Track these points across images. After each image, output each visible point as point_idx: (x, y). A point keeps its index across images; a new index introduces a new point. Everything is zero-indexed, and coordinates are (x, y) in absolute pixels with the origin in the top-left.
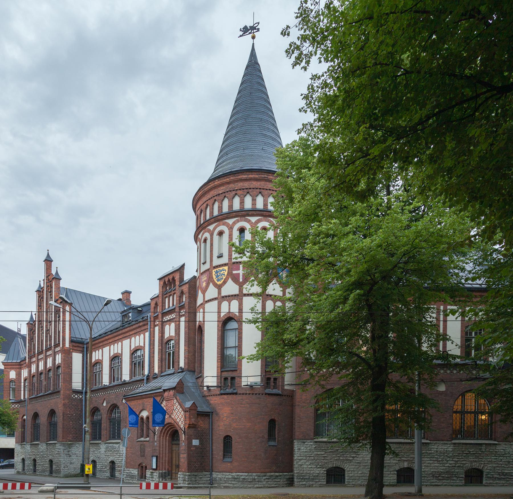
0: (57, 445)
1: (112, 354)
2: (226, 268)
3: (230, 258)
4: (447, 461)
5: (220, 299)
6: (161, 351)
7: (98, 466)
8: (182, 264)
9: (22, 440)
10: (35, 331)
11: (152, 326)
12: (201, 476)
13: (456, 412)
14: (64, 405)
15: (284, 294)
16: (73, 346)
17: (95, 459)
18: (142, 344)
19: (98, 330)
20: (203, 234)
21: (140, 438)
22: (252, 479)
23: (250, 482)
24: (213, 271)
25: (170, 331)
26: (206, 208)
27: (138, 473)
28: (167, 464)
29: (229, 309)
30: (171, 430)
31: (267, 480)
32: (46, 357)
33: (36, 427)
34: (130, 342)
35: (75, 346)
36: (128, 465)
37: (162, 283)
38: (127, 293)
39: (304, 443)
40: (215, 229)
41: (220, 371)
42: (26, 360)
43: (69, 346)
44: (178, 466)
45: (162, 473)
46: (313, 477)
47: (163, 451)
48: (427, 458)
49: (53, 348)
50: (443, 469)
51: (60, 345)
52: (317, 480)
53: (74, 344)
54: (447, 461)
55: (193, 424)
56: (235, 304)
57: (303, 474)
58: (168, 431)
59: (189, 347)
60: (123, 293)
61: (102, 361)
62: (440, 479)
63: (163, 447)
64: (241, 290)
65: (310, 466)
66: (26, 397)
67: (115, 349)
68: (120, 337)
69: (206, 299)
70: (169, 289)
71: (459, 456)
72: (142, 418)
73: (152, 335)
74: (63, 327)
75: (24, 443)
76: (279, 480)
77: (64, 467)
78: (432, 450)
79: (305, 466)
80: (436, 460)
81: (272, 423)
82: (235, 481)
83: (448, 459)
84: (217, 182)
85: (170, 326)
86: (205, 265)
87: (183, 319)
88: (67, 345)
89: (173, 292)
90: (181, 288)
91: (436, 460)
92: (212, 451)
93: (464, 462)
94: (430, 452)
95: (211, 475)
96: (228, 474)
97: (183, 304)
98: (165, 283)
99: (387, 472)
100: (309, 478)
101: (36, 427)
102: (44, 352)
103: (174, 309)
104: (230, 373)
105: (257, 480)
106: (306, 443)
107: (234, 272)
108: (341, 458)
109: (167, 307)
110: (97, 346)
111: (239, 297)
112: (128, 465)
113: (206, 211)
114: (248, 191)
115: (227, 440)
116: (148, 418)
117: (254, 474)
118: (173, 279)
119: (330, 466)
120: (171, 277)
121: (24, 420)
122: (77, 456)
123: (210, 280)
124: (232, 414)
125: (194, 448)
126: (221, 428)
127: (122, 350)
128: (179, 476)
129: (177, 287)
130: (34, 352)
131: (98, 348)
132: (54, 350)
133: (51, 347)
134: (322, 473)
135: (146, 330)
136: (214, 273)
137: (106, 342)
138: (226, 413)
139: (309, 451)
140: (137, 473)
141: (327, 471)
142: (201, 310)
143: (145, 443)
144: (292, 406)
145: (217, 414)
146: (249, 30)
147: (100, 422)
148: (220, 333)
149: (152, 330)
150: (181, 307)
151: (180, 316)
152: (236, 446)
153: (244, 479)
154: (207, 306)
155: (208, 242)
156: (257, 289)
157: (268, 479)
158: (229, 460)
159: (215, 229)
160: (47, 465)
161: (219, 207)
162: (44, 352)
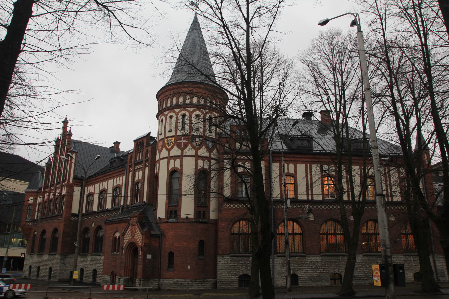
0: (56, 256)
1: (101, 189)
2: (173, 138)
3: (176, 133)
4: (318, 269)
5: (170, 158)
6: (132, 189)
7: (85, 273)
8: (149, 132)
9: (31, 251)
10: (50, 169)
11: (128, 172)
12: (152, 282)
13: (322, 234)
14: (65, 225)
15: (210, 155)
16: (75, 182)
17: (83, 267)
18: (121, 184)
19: (91, 173)
20: (161, 116)
21: (114, 252)
22: (187, 283)
23: (185, 286)
24: (166, 140)
25: (139, 176)
26: (163, 102)
27: (110, 279)
28: (130, 272)
29: (175, 165)
30: (134, 247)
31: (197, 285)
32: (56, 189)
33: (43, 241)
34: (113, 182)
35: (77, 182)
36: (104, 273)
37: (136, 144)
38: (117, 144)
39: (223, 257)
40: (168, 114)
41: (167, 206)
42: (42, 189)
43: (73, 182)
44: (136, 274)
45: (126, 279)
46: (229, 282)
47: (127, 262)
48: (305, 267)
49: (61, 183)
50: (315, 275)
51: (66, 181)
52: (232, 284)
53: (76, 180)
54: (318, 269)
55: (147, 243)
56: (178, 161)
57: (223, 280)
58: (131, 248)
59: (149, 188)
60: (114, 143)
61: (94, 193)
62: (314, 282)
63: (127, 260)
64: (182, 153)
65: (227, 274)
66: (39, 217)
67: (103, 185)
68: (107, 177)
69: (161, 157)
70: (140, 148)
71: (326, 265)
72: (116, 237)
73: (127, 178)
74: (69, 169)
75: (33, 253)
76: (206, 284)
77: (60, 273)
78: (308, 261)
79: (224, 274)
80: (311, 268)
81: (202, 243)
82: (175, 285)
83: (319, 267)
84: (170, 88)
85: (139, 172)
86: (161, 135)
87: (147, 169)
88: (71, 181)
89: (142, 150)
90: (147, 148)
91: (311, 268)
92: (161, 263)
93: (329, 269)
94: (307, 262)
95: (159, 280)
96: (170, 280)
97: (147, 158)
98: (137, 143)
99: (279, 278)
100: (227, 283)
101: (43, 241)
102: (55, 185)
103: (142, 161)
104: (174, 207)
105: (190, 285)
106: (224, 258)
107: (179, 141)
108: (248, 268)
109: (138, 160)
110: (92, 182)
111: (181, 157)
112: (104, 273)
113: (163, 103)
114: (187, 93)
115: (171, 255)
116: (119, 237)
117: (188, 280)
118: (143, 141)
119: (241, 274)
120: (141, 140)
121: (35, 235)
122: (70, 265)
123: (163, 145)
124: (175, 236)
125: (148, 261)
126: (167, 246)
127: (108, 186)
128: (136, 281)
129: (145, 147)
130: (48, 184)
131: (92, 184)
132: (62, 184)
133: (60, 182)
134: (236, 279)
135: (123, 174)
136: (166, 141)
137: (98, 180)
138: (170, 235)
139: (226, 263)
140: (110, 278)
141: (239, 277)
142: (158, 164)
143: (116, 256)
144: (216, 231)
145: (165, 236)
146: (194, 4)
147: (89, 238)
148: (168, 180)
149: (127, 174)
150: (147, 161)
151: (146, 166)
152: (177, 260)
153: (181, 283)
154: (161, 162)
155: (164, 121)
156: (193, 152)
157: (198, 283)
158: (172, 270)
159: (168, 114)
160: (47, 272)
161: (170, 101)
162: (55, 185)
